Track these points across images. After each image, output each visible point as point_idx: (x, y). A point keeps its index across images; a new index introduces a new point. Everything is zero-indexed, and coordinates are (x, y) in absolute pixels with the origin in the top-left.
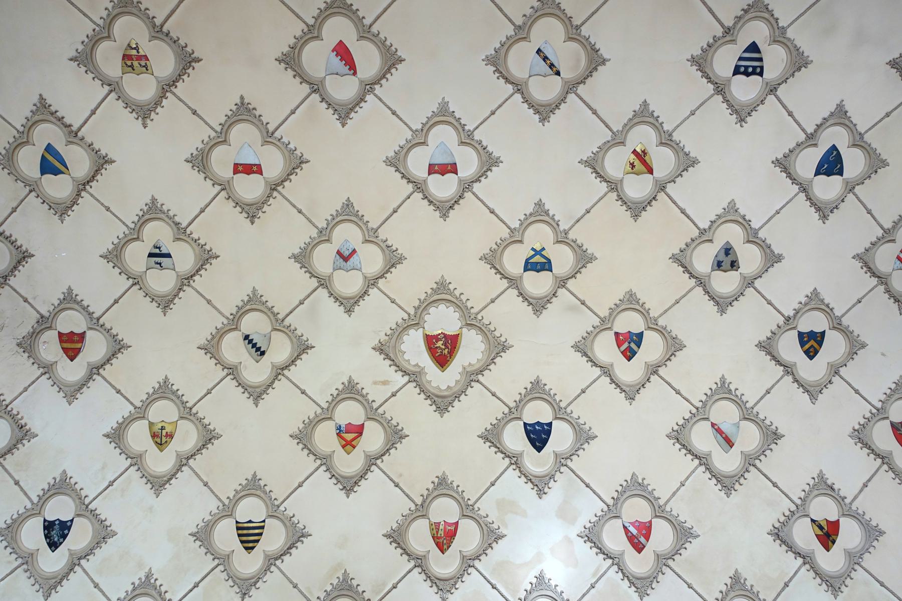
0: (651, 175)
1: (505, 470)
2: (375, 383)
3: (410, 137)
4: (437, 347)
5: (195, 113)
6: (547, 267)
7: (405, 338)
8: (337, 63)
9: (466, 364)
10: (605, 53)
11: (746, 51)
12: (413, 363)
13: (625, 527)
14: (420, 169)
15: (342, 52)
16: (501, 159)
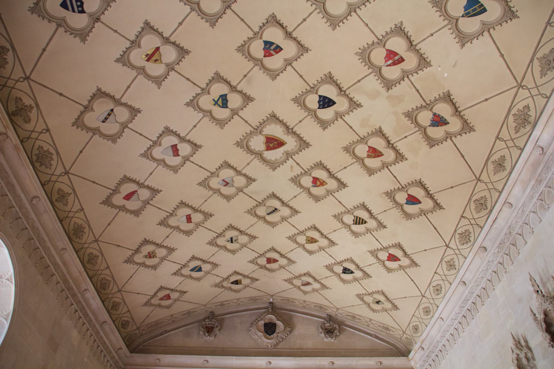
0: (160, 48)
1: (344, 121)
2: (292, 171)
3: (162, 166)
4: (273, 146)
5: (167, 237)
6: (224, 98)
7: (268, 158)
8: (134, 197)
9: (283, 133)
10: (94, 90)
11: (68, 9)
12: (282, 155)
13: (387, 66)
14: (177, 161)
15: (128, 197)
16: (165, 126)
